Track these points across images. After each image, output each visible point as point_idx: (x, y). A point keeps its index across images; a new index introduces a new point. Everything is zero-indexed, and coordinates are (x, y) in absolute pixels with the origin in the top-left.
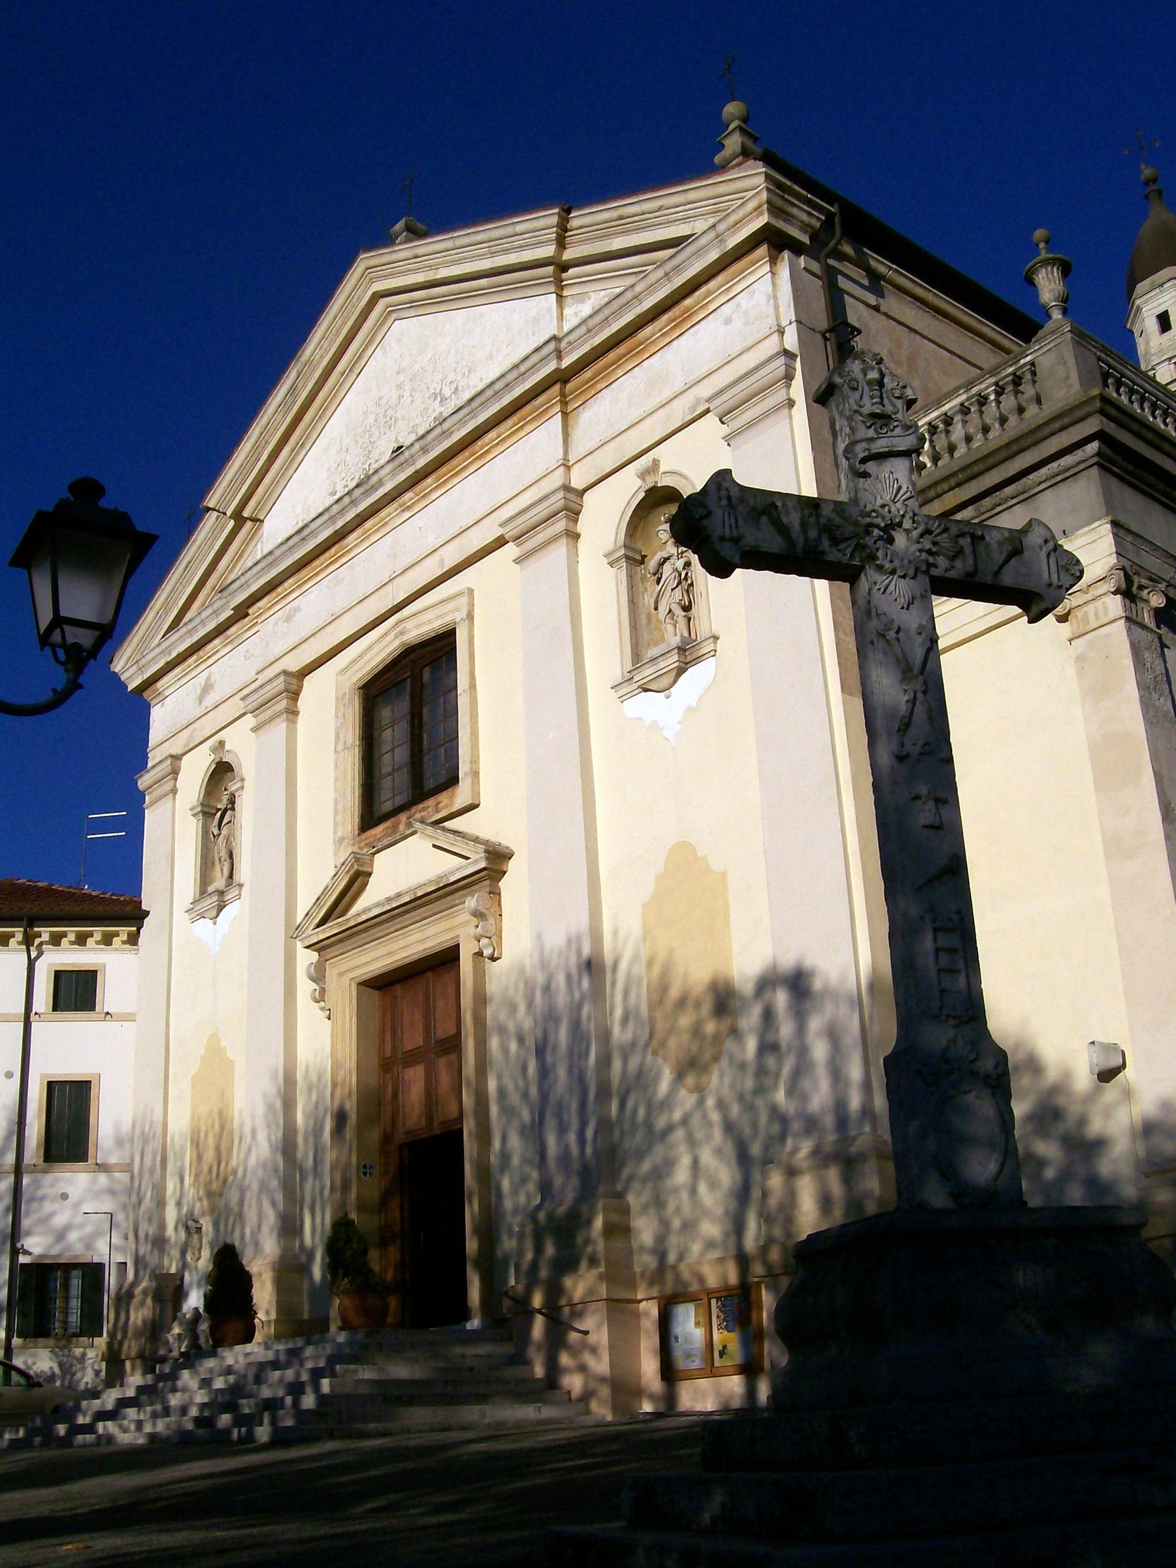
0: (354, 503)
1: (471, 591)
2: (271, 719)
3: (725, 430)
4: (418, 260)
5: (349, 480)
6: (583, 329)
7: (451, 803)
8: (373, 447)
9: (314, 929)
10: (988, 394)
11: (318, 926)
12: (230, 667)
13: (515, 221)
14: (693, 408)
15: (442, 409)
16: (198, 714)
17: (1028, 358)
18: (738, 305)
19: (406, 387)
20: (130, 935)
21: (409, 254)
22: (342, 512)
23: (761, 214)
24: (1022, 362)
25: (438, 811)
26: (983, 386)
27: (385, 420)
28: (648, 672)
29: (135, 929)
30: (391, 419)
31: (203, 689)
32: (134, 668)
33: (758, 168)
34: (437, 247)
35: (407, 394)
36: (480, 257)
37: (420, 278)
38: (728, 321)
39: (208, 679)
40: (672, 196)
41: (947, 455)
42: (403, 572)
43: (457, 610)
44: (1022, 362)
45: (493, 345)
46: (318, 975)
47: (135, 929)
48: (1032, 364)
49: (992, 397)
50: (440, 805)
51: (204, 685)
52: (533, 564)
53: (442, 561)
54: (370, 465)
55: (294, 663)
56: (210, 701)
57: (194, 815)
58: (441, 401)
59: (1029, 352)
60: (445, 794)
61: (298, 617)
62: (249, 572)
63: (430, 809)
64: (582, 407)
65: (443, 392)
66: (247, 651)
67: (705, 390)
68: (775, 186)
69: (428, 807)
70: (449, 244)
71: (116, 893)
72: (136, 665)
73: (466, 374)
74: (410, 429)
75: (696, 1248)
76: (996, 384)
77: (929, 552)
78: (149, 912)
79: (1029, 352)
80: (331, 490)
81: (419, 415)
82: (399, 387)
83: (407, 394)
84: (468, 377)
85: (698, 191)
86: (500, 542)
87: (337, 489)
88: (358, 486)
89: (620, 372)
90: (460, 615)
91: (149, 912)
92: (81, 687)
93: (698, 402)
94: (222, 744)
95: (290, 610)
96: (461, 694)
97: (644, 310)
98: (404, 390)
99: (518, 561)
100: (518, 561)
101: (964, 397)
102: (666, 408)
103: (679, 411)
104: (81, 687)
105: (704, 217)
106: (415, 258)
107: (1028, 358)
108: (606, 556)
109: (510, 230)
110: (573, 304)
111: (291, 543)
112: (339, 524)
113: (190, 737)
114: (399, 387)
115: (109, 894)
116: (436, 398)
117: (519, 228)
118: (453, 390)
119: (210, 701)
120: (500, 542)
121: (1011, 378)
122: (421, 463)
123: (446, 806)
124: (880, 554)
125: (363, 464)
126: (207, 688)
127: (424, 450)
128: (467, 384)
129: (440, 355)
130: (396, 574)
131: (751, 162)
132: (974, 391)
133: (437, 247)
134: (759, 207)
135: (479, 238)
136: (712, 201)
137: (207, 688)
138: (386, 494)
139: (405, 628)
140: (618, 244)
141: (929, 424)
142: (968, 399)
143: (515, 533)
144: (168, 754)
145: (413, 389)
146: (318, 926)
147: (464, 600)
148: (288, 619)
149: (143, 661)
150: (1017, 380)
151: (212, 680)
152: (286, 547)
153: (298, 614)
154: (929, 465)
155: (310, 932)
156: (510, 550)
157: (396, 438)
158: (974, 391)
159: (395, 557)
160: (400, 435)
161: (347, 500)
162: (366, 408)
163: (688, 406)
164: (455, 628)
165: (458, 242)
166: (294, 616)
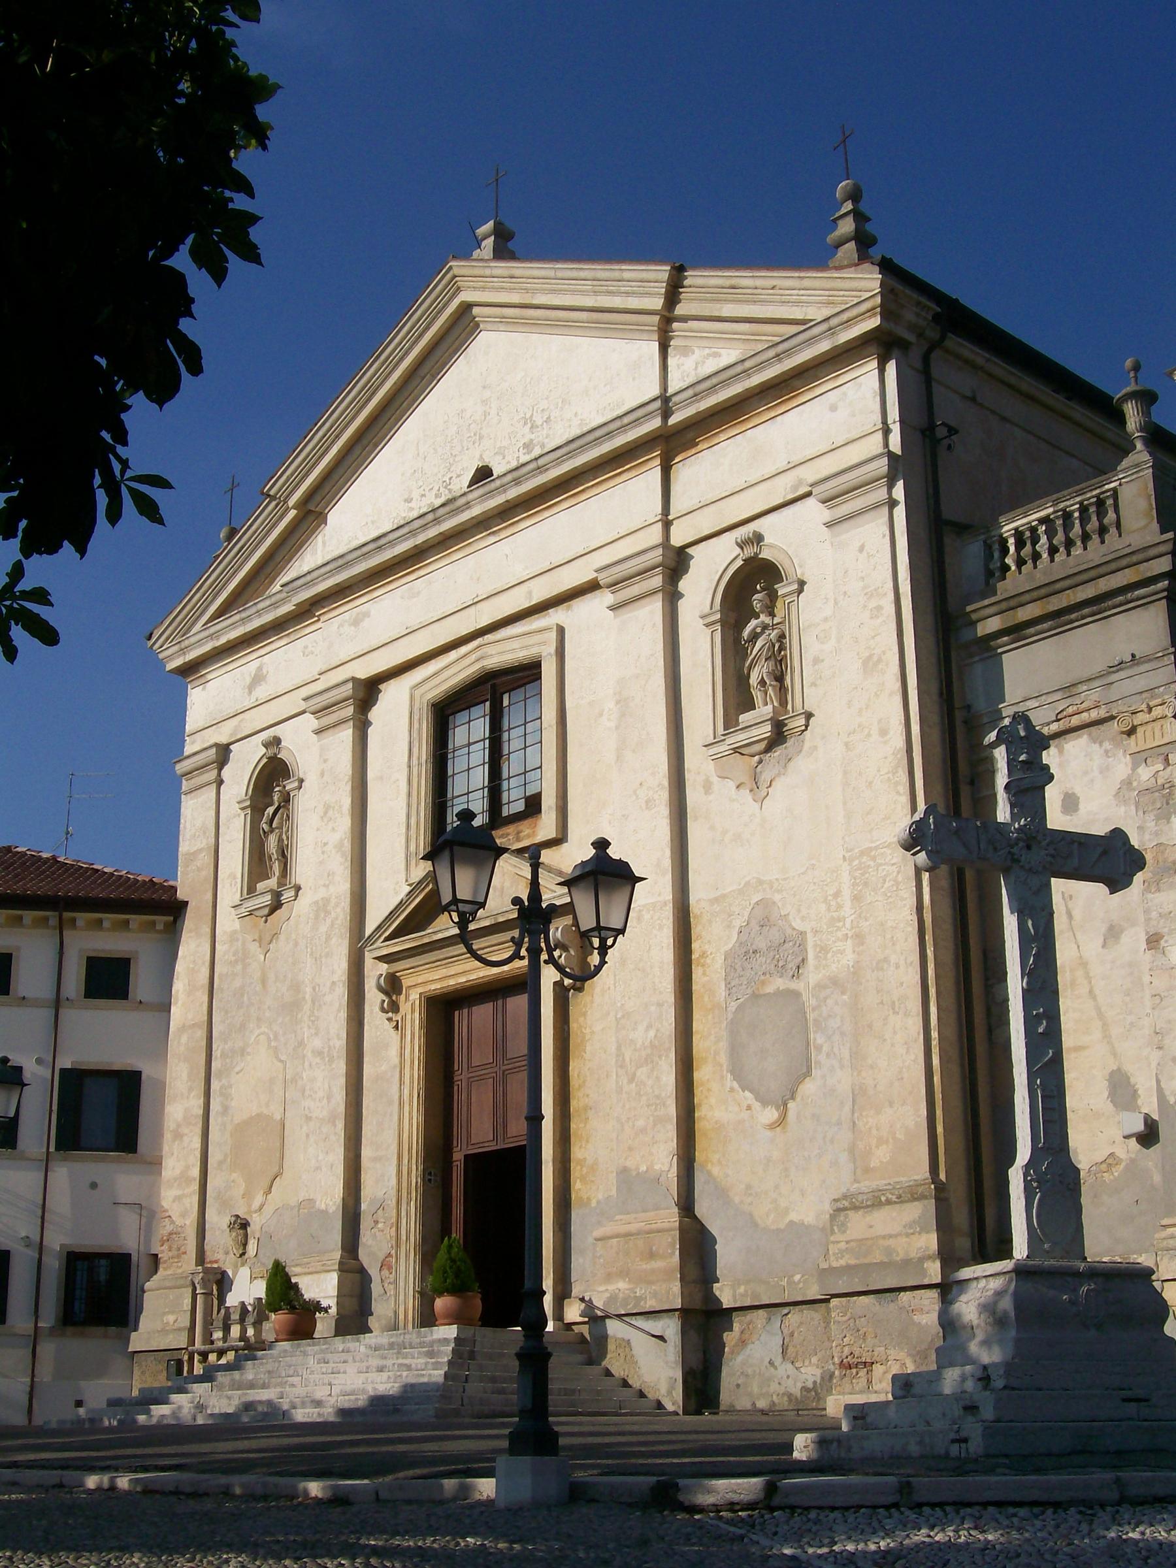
0: (437, 521)
1: (561, 631)
2: (335, 725)
3: (826, 514)
4: (514, 280)
5: (427, 490)
6: (690, 392)
7: (534, 834)
8: (454, 460)
9: (383, 942)
10: (1074, 511)
11: (387, 939)
12: (285, 661)
13: (623, 267)
14: (795, 488)
15: (533, 436)
16: (248, 704)
17: (1112, 485)
18: (845, 394)
19: (492, 405)
20: (166, 924)
21: (506, 273)
22: (425, 527)
23: (874, 315)
24: (1107, 487)
25: (518, 840)
26: (1068, 503)
27: (469, 435)
28: (740, 738)
29: (172, 918)
30: (475, 435)
31: (253, 679)
32: (176, 648)
33: (871, 273)
34: (536, 273)
35: (493, 412)
36: (583, 293)
37: (515, 298)
38: (833, 408)
39: (260, 668)
40: (787, 279)
41: (1031, 561)
42: (488, 598)
43: (544, 643)
44: (1107, 487)
45: (590, 381)
46: (392, 986)
47: (172, 918)
48: (1115, 490)
49: (1076, 514)
50: (522, 835)
51: (255, 675)
52: (628, 614)
53: (530, 593)
54: (450, 479)
55: (365, 670)
56: (262, 692)
57: (243, 809)
58: (532, 427)
59: (1114, 479)
60: (526, 822)
61: (366, 623)
62: (317, 571)
63: (511, 837)
64: (681, 463)
65: (534, 419)
66: (306, 647)
67: (810, 474)
68: (887, 291)
69: (508, 834)
70: (551, 273)
71: (131, 872)
72: (178, 645)
73: (560, 405)
74: (496, 450)
75: (629, 1261)
76: (1081, 503)
77: (1053, 856)
78: (187, 902)
79: (1114, 479)
80: (406, 497)
81: (507, 437)
82: (484, 402)
83: (493, 412)
84: (562, 409)
85: (813, 279)
86: (592, 586)
87: (412, 496)
88: (443, 505)
89: (723, 437)
90: (547, 652)
91: (187, 902)
92: (606, 962)
93: (800, 482)
94: (277, 741)
95: (358, 614)
96: (546, 728)
97: (753, 385)
98: (490, 408)
99: (613, 608)
100: (613, 608)
101: (1051, 510)
102: (769, 483)
103: (780, 491)
104: (606, 962)
105: (817, 305)
106: (511, 278)
107: (1112, 485)
108: (702, 617)
109: (617, 275)
110: (675, 356)
111: (365, 549)
112: (420, 539)
113: (237, 729)
114: (484, 402)
115: (125, 872)
116: (525, 423)
117: (626, 275)
118: (545, 419)
119: (262, 692)
120: (592, 586)
121: (1095, 499)
122: (513, 493)
123: (528, 836)
124: (1023, 858)
125: (444, 476)
126: (258, 679)
127: (517, 481)
128: (561, 416)
129: (532, 379)
130: (479, 599)
131: (867, 266)
132: (1062, 505)
133: (536, 273)
134: (874, 308)
135: (582, 274)
136: (827, 293)
137: (258, 679)
138: (473, 518)
139: (487, 652)
140: (728, 310)
141: (1016, 529)
142: (1055, 512)
143: (609, 580)
144: (212, 742)
145: (500, 409)
146: (387, 939)
147: (553, 635)
148: (356, 623)
149: (186, 643)
150: (1100, 503)
151: (265, 671)
152: (359, 553)
153: (367, 620)
154: (1013, 568)
155: (378, 944)
156: (605, 598)
157: (481, 456)
158: (1062, 505)
159: (478, 579)
160: (487, 452)
161: (430, 517)
162: (446, 418)
163: (789, 486)
164: (541, 661)
165: (560, 274)
166: (362, 620)
